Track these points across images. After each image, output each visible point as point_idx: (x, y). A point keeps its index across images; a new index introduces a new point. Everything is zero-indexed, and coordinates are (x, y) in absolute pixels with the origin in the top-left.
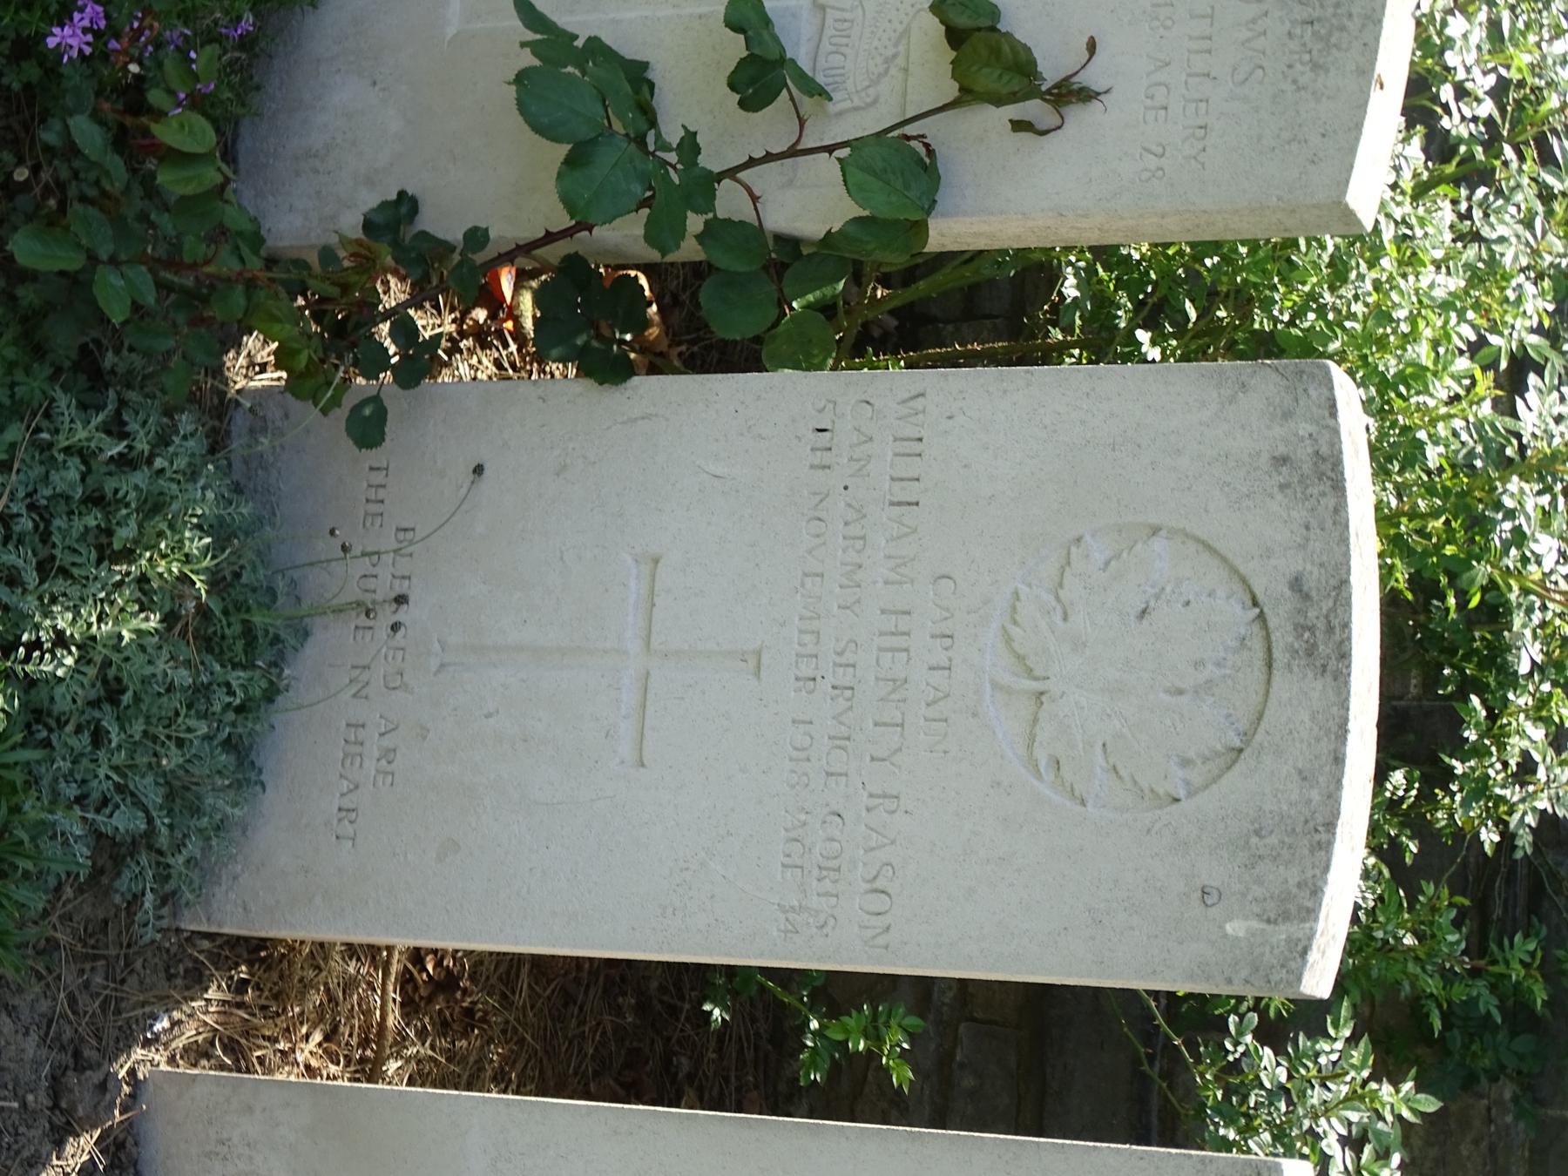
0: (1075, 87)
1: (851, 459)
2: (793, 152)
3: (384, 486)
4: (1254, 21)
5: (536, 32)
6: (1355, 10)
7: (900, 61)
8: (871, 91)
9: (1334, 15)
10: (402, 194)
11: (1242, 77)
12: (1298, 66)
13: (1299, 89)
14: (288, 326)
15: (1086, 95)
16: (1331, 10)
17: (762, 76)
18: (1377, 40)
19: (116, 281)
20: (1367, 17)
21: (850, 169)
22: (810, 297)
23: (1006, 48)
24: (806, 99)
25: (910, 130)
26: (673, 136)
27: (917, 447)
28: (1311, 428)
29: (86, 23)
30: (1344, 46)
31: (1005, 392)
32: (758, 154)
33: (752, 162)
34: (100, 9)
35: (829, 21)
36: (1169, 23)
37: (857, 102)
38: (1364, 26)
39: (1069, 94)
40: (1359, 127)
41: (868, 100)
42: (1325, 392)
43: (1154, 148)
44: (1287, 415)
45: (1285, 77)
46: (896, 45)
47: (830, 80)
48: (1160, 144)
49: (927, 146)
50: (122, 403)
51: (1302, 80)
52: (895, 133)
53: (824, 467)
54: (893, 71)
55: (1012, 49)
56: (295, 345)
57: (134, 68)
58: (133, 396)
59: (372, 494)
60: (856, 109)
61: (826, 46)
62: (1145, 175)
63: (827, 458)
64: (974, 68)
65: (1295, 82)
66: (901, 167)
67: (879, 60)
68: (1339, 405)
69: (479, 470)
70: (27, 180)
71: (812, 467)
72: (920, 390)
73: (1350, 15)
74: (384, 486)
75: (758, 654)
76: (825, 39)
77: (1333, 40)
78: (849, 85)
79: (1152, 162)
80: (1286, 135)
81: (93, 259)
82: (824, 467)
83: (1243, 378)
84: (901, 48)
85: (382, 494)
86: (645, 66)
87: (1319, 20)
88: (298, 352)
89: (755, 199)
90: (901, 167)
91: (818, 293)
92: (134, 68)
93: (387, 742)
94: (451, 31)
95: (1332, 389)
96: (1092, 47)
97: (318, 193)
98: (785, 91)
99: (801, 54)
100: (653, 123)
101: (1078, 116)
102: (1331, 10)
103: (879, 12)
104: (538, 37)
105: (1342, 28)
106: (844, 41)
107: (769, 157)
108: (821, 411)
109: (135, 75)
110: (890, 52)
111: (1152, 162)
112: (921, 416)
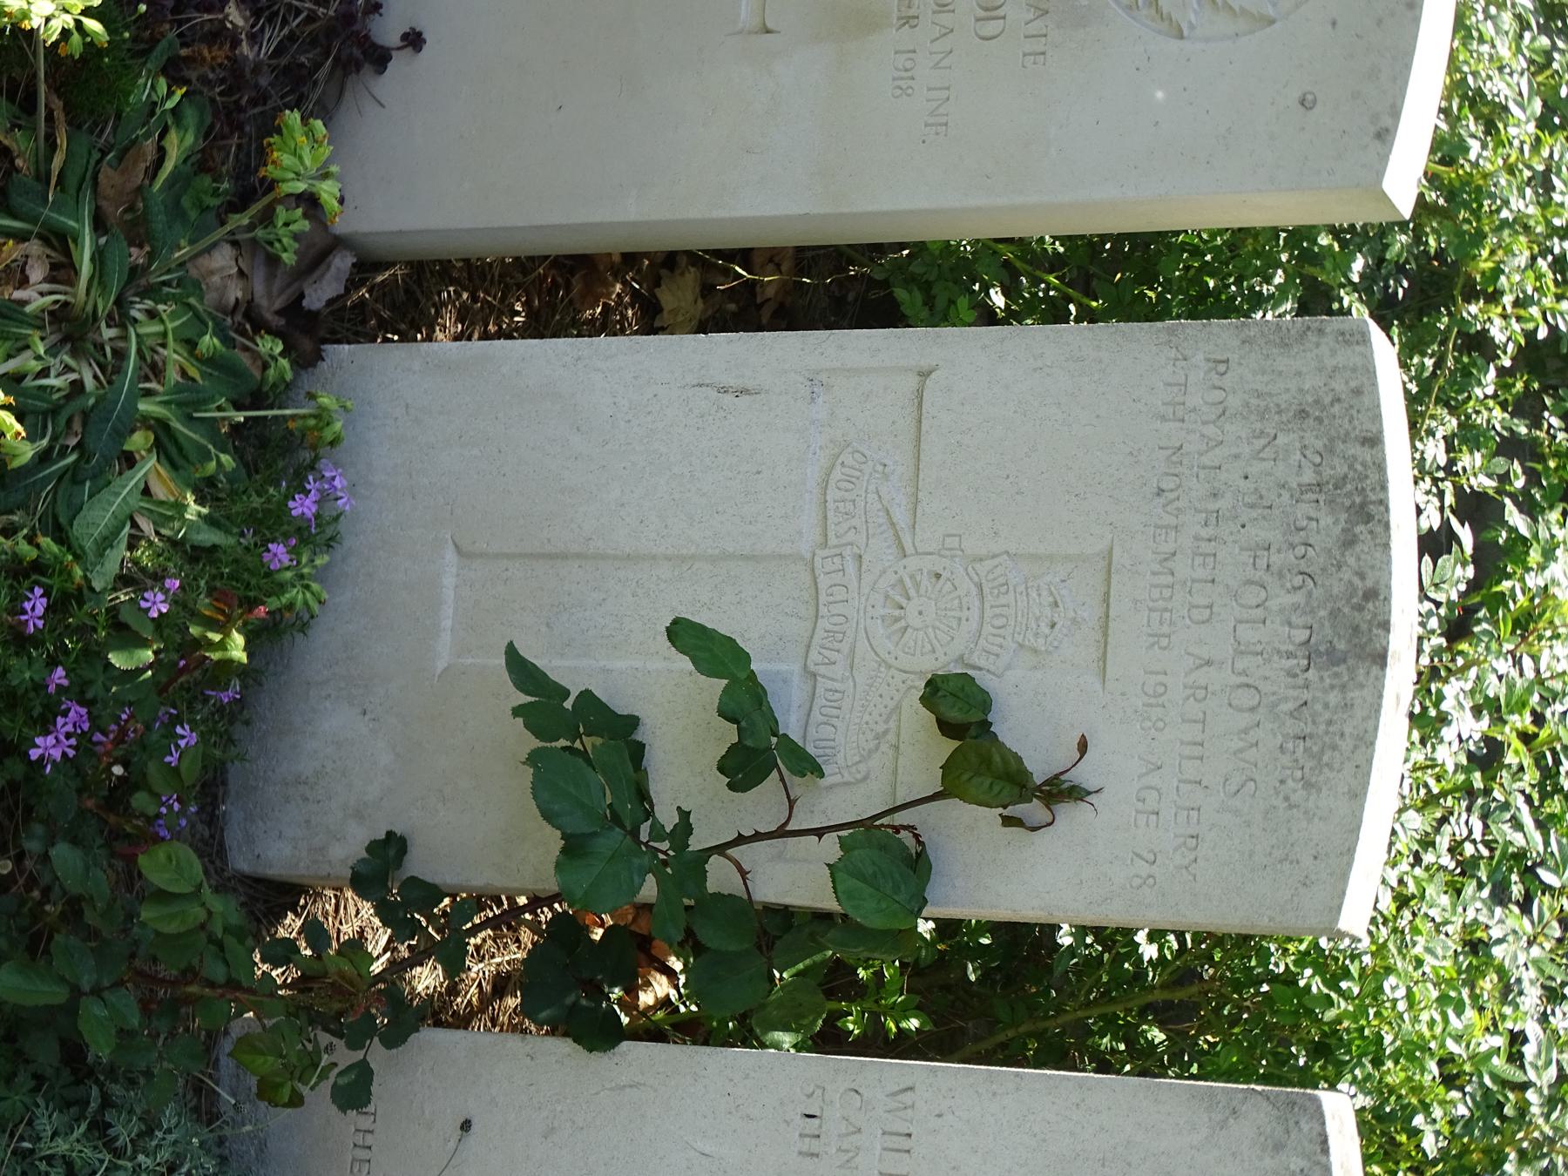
0: (1066, 785)
1: (839, 1149)
2: (782, 833)
3: (371, 1132)
4: (1246, 731)
5: (528, 693)
6: (1347, 730)
7: (891, 737)
8: (862, 767)
9: (1327, 733)
10: (390, 834)
11: (1234, 788)
12: (1290, 782)
13: (1291, 807)
14: (271, 1059)
15: (1076, 794)
16: (1323, 727)
17: (758, 751)
18: (1370, 761)
19: (99, 1011)
20: (1360, 738)
21: (839, 875)
22: (801, 966)
23: (997, 758)
24: (797, 780)
25: (885, 821)
26: (669, 819)
27: (904, 1143)
28: (1302, 1163)
29: (70, 728)
30: (1336, 766)
31: (994, 1094)
32: (747, 833)
33: (740, 840)
34: (84, 711)
35: (820, 691)
36: (1160, 724)
37: (847, 778)
38: (1356, 747)
39: (1060, 791)
40: (1351, 851)
41: (859, 776)
42: (1317, 1128)
43: (1145, 854)
44: (1278, 1147)
45: (1277, 793)
46: (886, 722)
47: (821, 752)
48: (1151, 851)
49: (917, 836)
50: (106, 1102)
51: (1294, 798)
52: (885, 821)
53: (812, 1155)
54: (884, 747)
55: (1003, 758)
56: (278, 1080)
57: (118, 770)
58: (116, 1090)
59: (359, 1139)
60: (847, 784)
61: (816, 716)
62: (1137, 881)
63: (815, 1146)
64: (965, 777)
65: (1287, 799)
66: (888, 855)
67: (870, 736)
68: (1332, 1142)
69: (466, 1126)
70: (11, 873)
71: (800, 1153)
72: (909, 1084)
73: (1342, 735)
74: (371, 1132)
76: (816, 709)
77: (1325, 759)
78: (840, 758)
79: (1144, 869)
80: (1277, 853)
81: (76, 992)
82: (812, 1155)
83: (1234, 1103)
84: (892, 724)
85: (369, 1139)
86: (633, 722)
87: (1311, 736)
88: (282, 1085)
89: (743, 874)
90: (888, 855)
91: (808, 962)
92: (118, 770)
94: (441, 665)
95: (1324, 1123)
96: (1083, 747)
97: (308, 822)
98: (775, 773)
99: (791, 726)
100: (649, 814)
101: (1068, 813)
102: (1323, 727)
103: (871, 686)
104: (533, 699)
105: (1334, 748)
106: (835, 712)
107: (758, 836)
108: (810, 1096)
109: (118, 778)
110: (881, 728)
111: (1144, 869)
112: (909, 1111)
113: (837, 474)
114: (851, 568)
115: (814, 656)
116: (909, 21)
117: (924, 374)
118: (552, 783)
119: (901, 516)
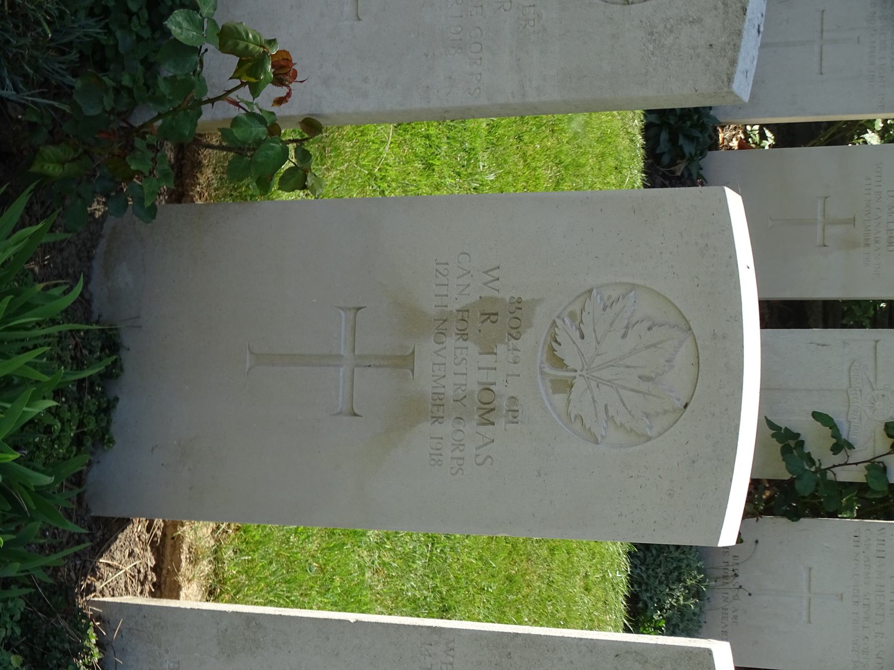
2: (846, 464)
17: (840, 445)
25: (877, 460)
33: (834, 466)
63: (858, 544)
69: (757, 542)
75: (842, 595)
86: (798, 435)
93: (735, 614)
107: (840, 465)
113: (853, 368)
114: (858, 393)
115: (849, 417)
116: (867, 245)
117: (877, 341)
118: (786, 451)
119: (872, 379)
